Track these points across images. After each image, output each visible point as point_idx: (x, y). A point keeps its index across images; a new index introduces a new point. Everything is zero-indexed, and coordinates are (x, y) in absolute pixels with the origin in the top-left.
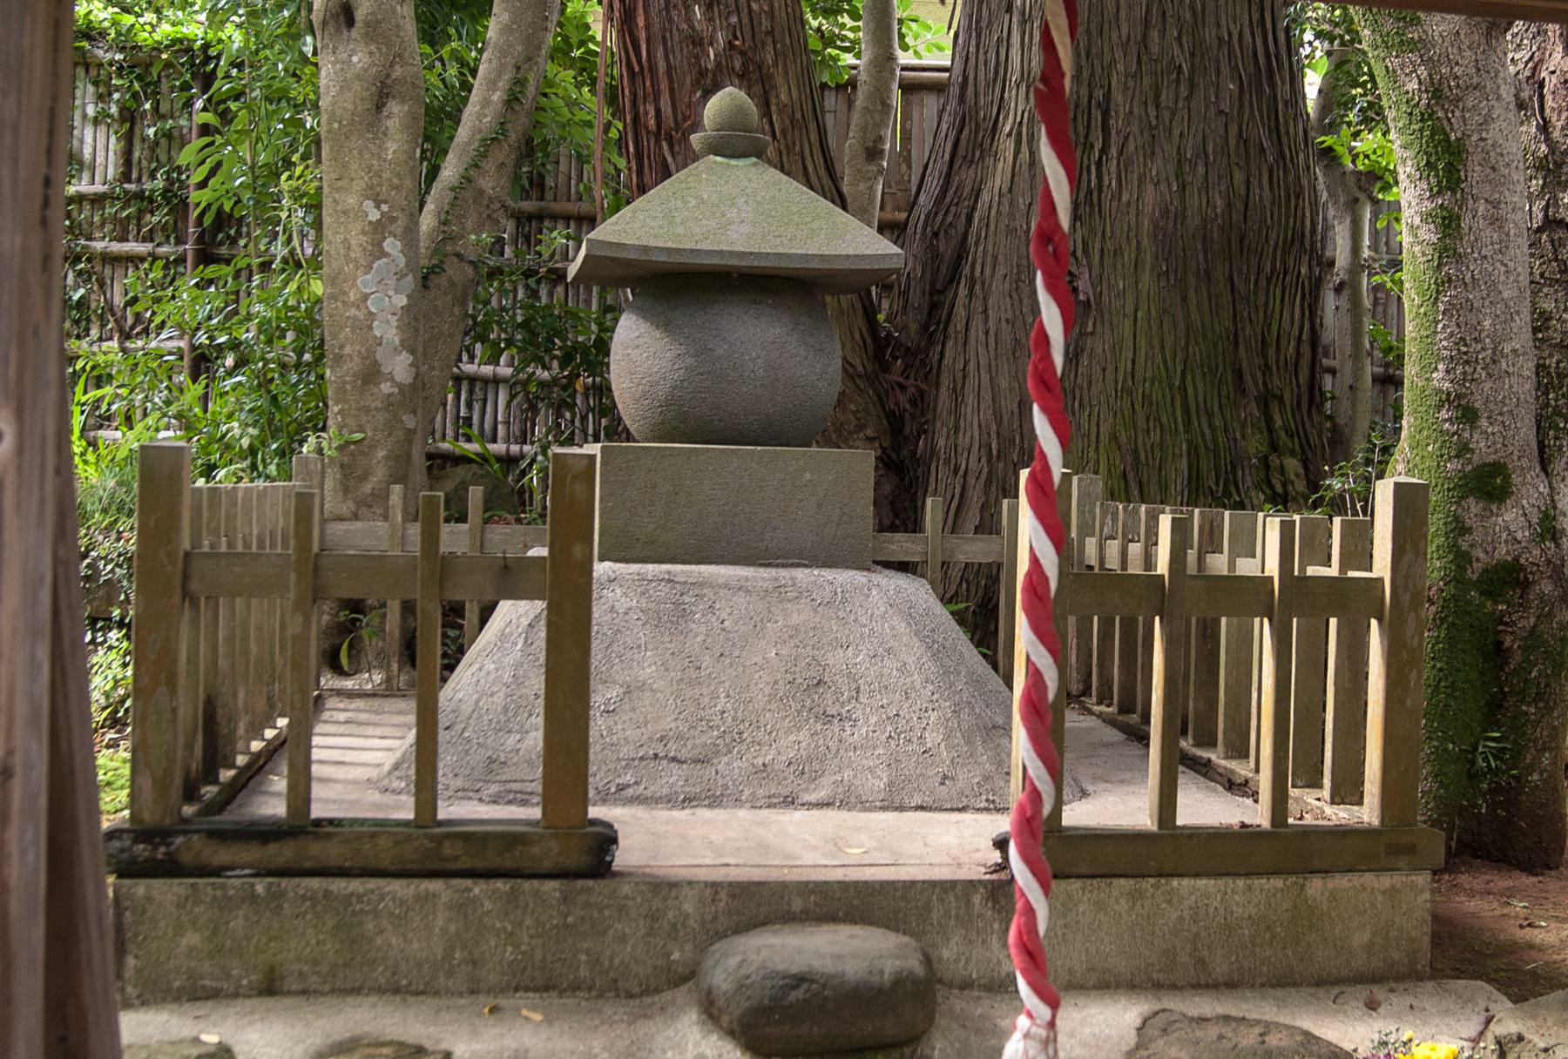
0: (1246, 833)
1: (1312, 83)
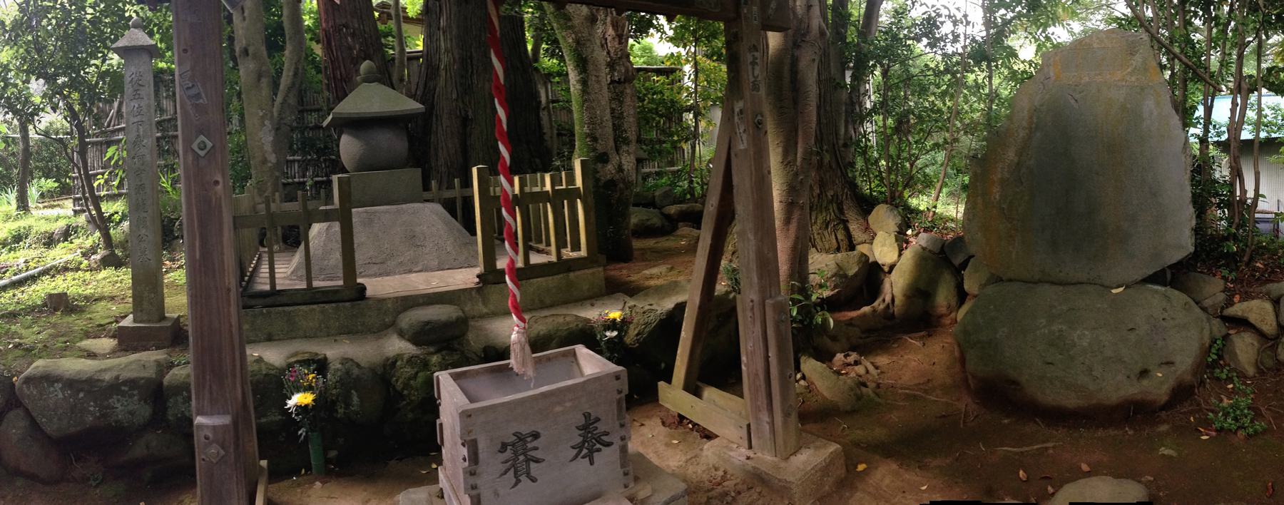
0: (550, 264)
1: (529, 47)
